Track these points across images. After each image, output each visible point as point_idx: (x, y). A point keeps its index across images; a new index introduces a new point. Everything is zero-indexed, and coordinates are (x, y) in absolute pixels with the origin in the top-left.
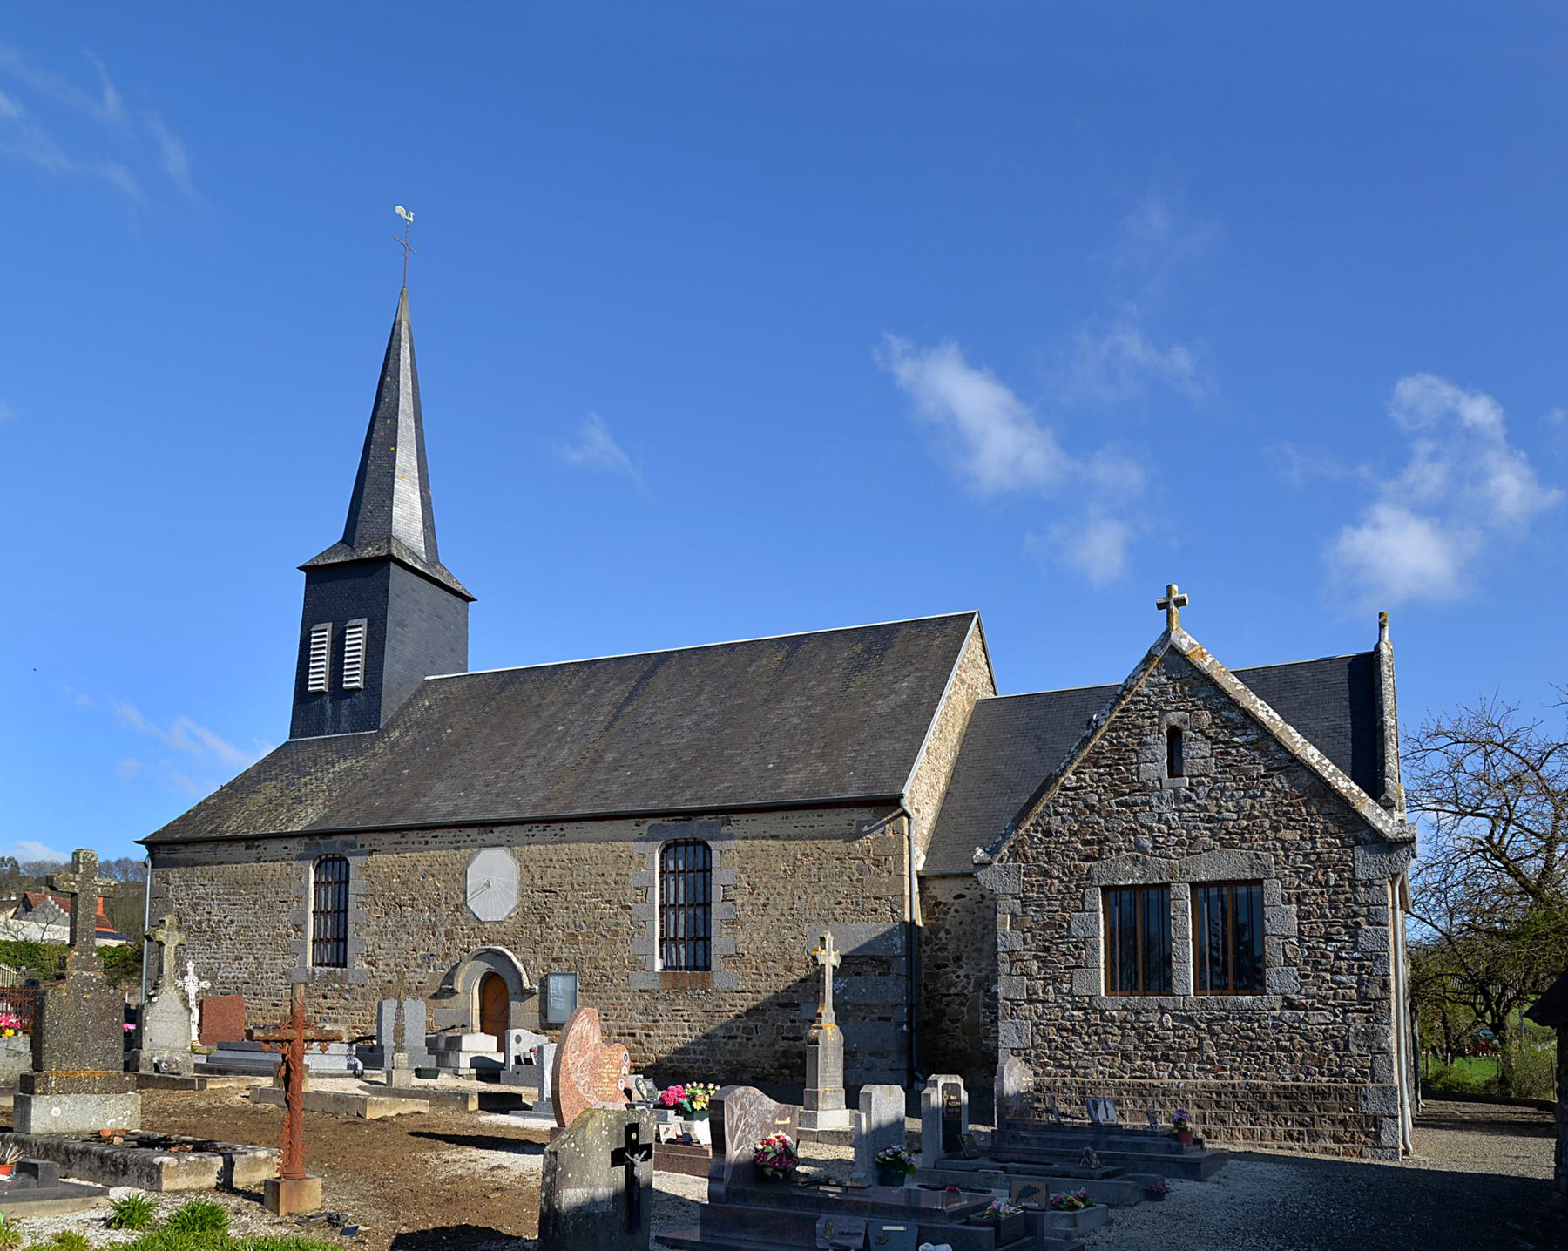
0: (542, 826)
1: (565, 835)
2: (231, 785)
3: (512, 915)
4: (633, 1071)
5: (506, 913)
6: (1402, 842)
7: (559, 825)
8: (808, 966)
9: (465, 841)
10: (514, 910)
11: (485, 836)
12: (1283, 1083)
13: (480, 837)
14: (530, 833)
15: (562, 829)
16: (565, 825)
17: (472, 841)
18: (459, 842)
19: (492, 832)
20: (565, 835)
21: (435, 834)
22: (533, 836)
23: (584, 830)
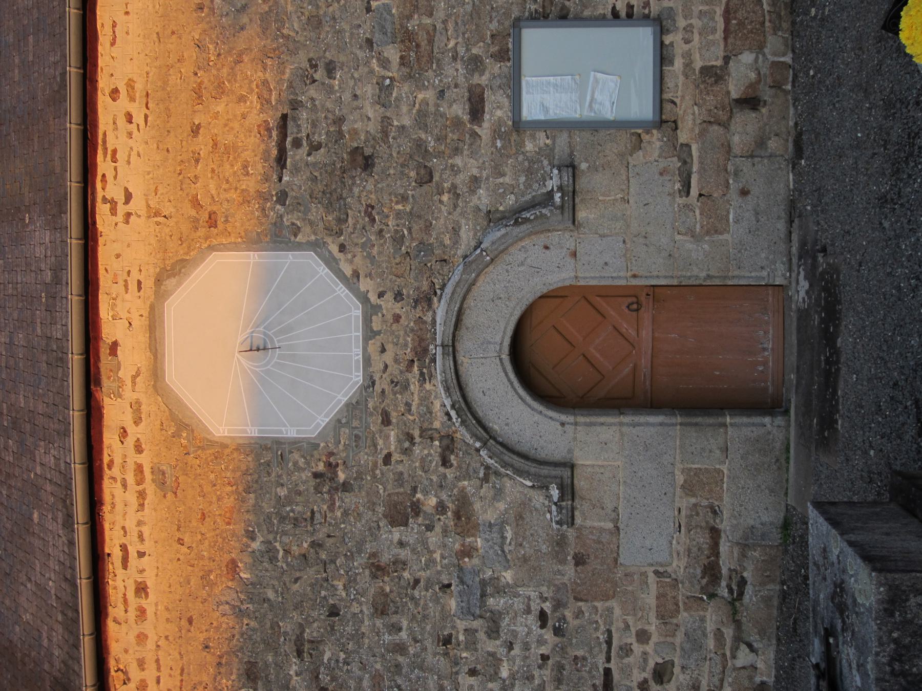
0: (103, 165)
1: (130, 85)
2: (128, 557)
3: (348, 271)
4: (495, 635)
5: (342, 290)
6: (855, 546)
7: (103, 101)
8: (333, 171)
9: (139, 449)
10: (331, 263)
11: (126, 373)
12: (840, 643)
13: (129, 395)
14: (121, 209)
15: (115, 93)
16: (104, 83)
17: (137, 421)
18: (139, 468)
19: (114, 346)
20: (130, 85)
21: (117, 554)
22: (128, 197)
23: (120, 18)
